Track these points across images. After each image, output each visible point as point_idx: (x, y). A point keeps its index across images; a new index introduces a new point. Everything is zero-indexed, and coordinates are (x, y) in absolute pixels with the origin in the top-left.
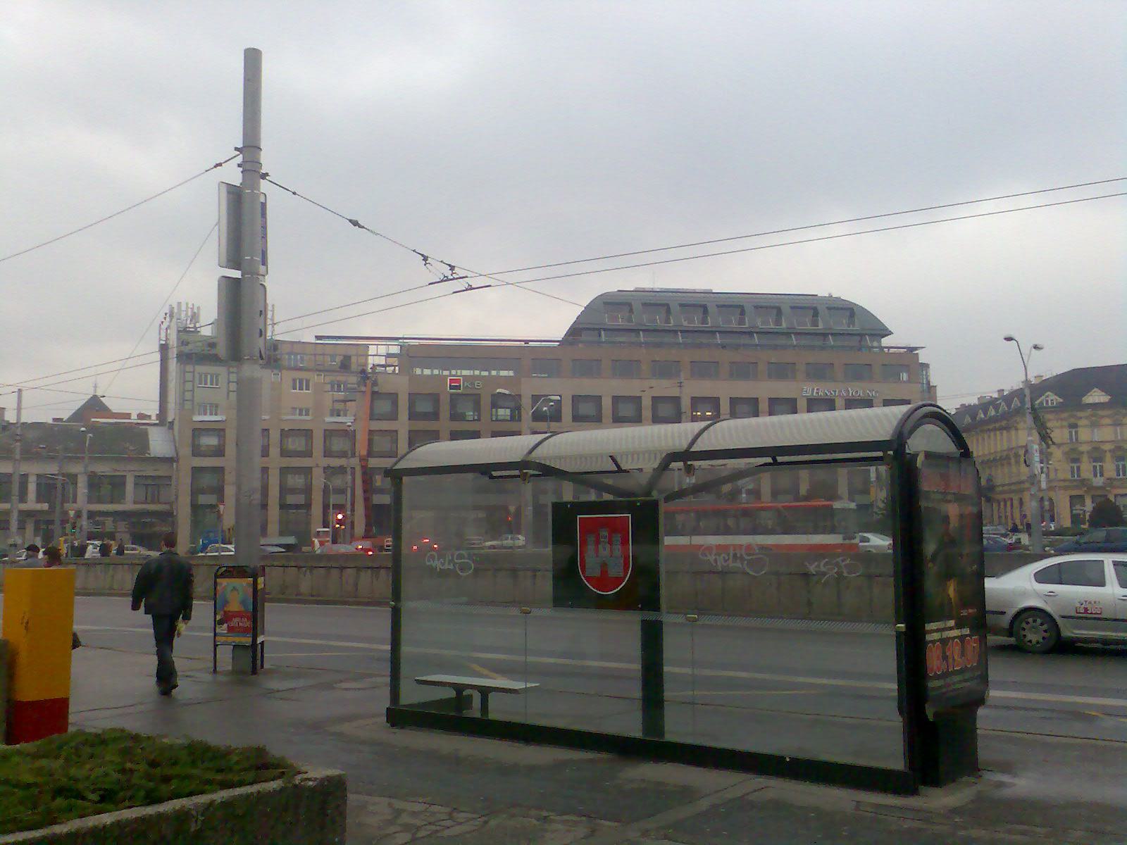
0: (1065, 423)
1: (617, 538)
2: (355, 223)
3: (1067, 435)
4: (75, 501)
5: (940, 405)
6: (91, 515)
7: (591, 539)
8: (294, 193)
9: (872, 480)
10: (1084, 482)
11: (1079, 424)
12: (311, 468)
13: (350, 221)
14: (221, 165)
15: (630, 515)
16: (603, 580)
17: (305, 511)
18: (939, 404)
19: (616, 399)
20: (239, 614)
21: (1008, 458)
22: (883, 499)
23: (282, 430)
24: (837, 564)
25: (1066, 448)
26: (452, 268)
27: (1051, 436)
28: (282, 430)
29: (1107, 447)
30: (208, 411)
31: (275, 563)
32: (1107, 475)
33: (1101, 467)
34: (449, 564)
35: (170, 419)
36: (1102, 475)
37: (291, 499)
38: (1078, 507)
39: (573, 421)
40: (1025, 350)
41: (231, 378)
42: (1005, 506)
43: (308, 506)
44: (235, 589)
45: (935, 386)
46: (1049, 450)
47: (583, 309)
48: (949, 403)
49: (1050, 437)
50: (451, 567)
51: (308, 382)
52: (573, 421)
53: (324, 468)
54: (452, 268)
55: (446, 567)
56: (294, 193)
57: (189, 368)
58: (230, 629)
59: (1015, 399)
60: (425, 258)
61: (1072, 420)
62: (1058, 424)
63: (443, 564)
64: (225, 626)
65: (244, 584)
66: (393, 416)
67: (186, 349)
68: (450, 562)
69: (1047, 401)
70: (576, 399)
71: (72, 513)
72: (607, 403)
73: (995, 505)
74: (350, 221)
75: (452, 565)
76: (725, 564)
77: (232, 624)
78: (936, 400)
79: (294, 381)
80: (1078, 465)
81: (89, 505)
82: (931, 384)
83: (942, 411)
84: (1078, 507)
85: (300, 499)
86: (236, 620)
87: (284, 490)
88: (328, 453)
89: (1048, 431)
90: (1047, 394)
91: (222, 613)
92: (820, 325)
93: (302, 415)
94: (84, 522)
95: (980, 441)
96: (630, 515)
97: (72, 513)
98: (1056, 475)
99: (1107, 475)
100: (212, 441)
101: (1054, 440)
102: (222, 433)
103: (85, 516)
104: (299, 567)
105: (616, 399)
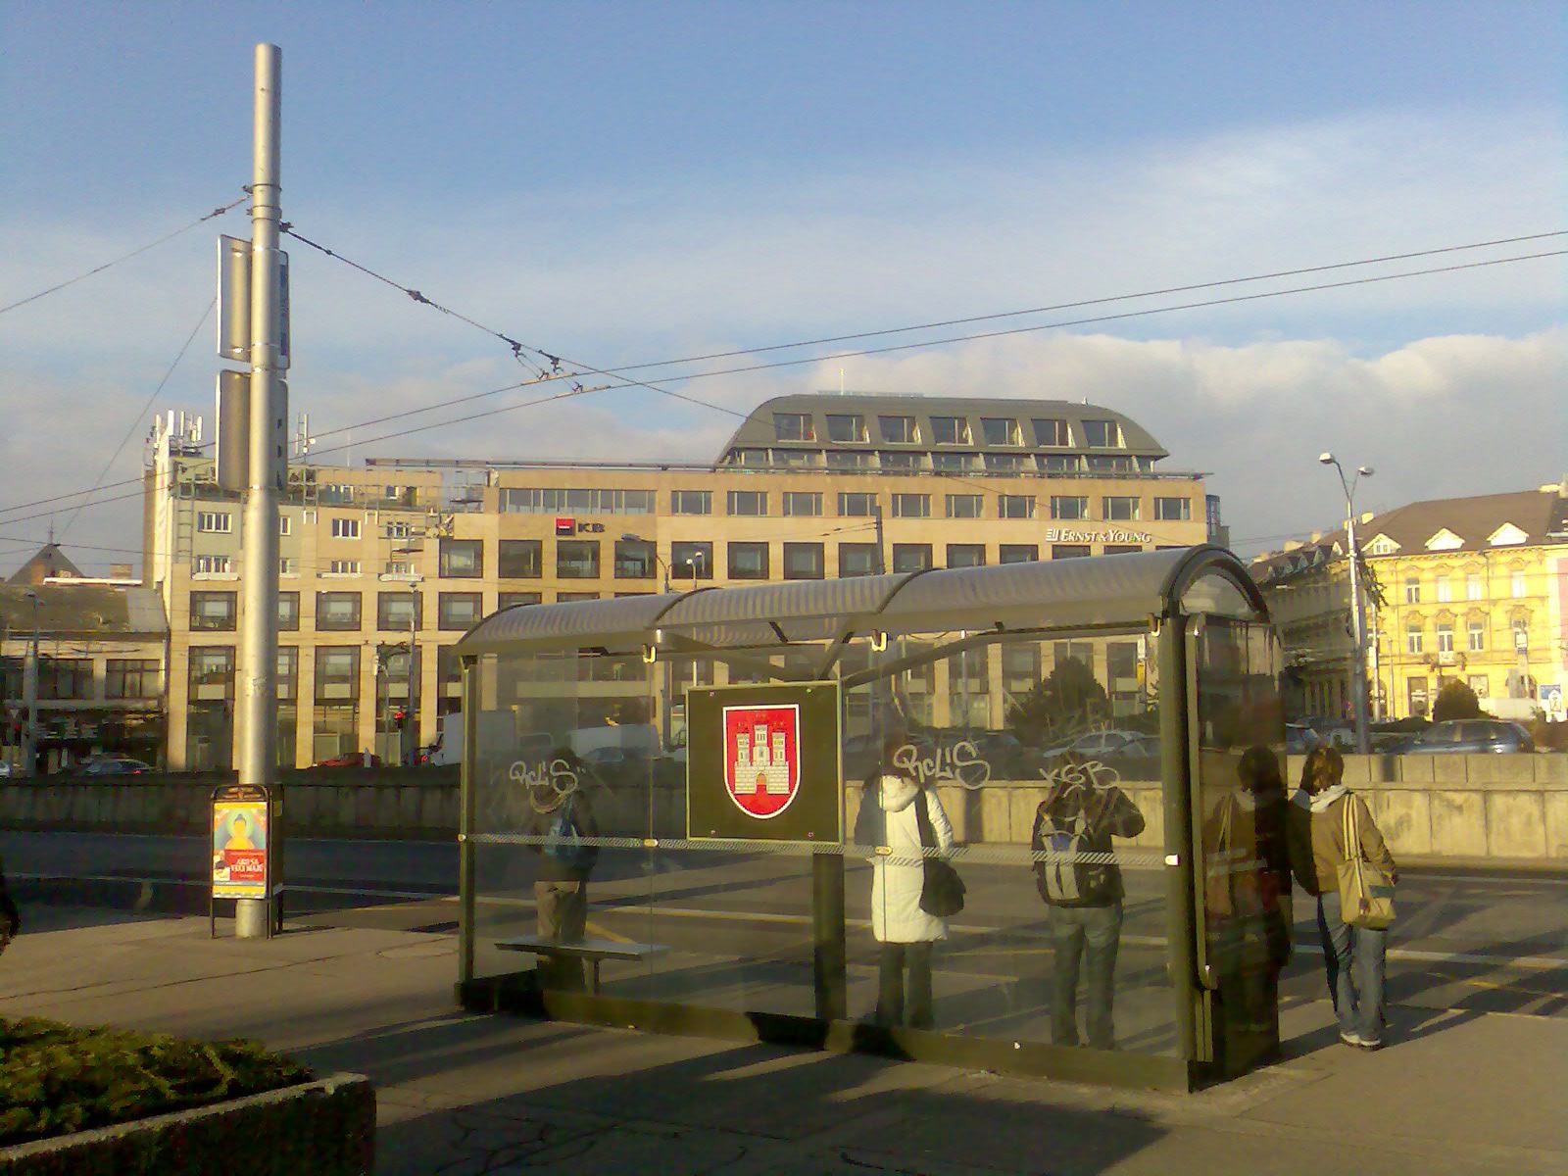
0: (1402, 578)
1: (779, 740)
2: (417, 296)
3: (1403, 593)
4: (19, 696)
5: (1234, 552)
6: (43, 715)
7: (743, 740)
8: (329, 252)
9: (1139, 657)
10: (1427, 659)
11: (1420, 578)
12: (360, 646)
13: (410, 292)
14: (223, 212)
15: (796, 706)
16: (761, 799)
17: (352, 707)
18: (1232, 549)
19: (789, 548)
20: (246, 854)
21: (1325, 625)
22: (1154, 683)
23: (318, 593)
24: (1084, 771)
25: (1403, 611)
26: (555, 360)
27: (1382, 594)
28: (318, 593)
29: (1458, 609)
30: (213, 565)
31: (305, 782)
32: (1426, 649)
33: (1419, 638)
34: (543, 779)
35: (157, 578)
36: (1451, 649)
37: (332, 691)
38: (1419, 692)
39: (730, 578)
40: (1349, 476)
41: (189, 532)
42: (1322, 690)
43: (354, 701)
44: (240, 818)
45: (1228, 527)
46: (1379, 614)
47: (744, 420)
48: (1252, 553)
49: (1381, 596)
50: (546, 782)
51: (355, 524)
52: (730, 578)
53: (378, 646)
54: (555, 360)
55: (539, 782)
56: (329, 252)
57: (186, 505)
58: (235, 876)
59: (1336, 544)
60: (517, 347)
61: (1412, 574)
62: (1393, 578)
63: (533, 779)
64: (227, 870)
65: (254, 811)
66: (477, 572)
67: (182, 478)
68: (547, 774)
69: (1378, 547)
70: (734, 548)
71: (14, 713)
72: (776, 554)
73: (1308, 689)
74: (410, 292)
75: (547, 779)
76: (929, 774)
77: (236, 868)
78: (1228, 546)
79: (335, 523)
80: (1450, 633)
81: (40, 701)
82: (1222, 525)
83: (1235, 560)
84: (1419, 692)
85: (343, 691)
86: (242, 862)
87: (321, 678)
88: (383, 624)
89: (1379, 587)
90: (1378, 537)
91: (222, 852)
92: (1070, 442)
93: (337, 571)
94: (31, 725)
95: (536, 626)
96: (796, 706)
97: (14, 713)
98: (1391, 649)
99: (1426, 649)
100: (219, 609)
101: (1387, 601)
102: (296, 597)
103: (33, 716)
104: (338, 787)
105: (789, 548)
